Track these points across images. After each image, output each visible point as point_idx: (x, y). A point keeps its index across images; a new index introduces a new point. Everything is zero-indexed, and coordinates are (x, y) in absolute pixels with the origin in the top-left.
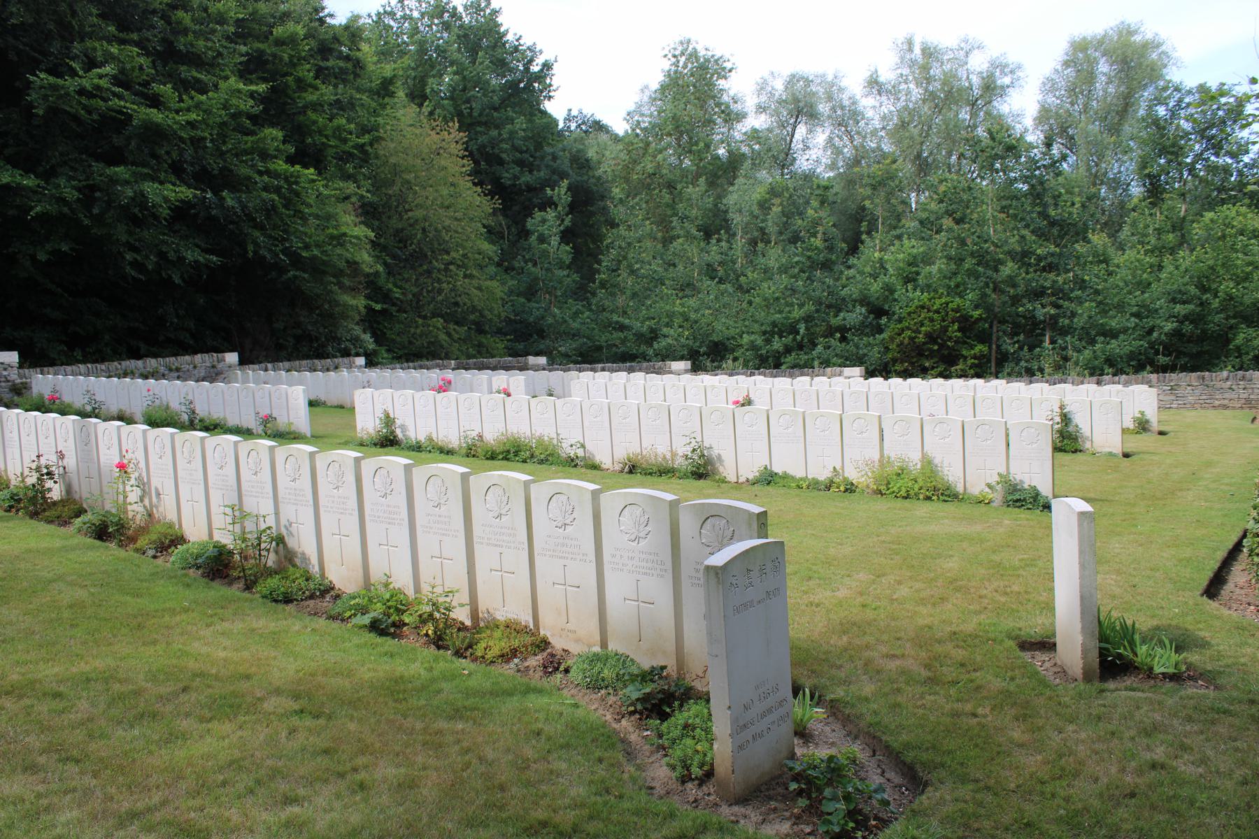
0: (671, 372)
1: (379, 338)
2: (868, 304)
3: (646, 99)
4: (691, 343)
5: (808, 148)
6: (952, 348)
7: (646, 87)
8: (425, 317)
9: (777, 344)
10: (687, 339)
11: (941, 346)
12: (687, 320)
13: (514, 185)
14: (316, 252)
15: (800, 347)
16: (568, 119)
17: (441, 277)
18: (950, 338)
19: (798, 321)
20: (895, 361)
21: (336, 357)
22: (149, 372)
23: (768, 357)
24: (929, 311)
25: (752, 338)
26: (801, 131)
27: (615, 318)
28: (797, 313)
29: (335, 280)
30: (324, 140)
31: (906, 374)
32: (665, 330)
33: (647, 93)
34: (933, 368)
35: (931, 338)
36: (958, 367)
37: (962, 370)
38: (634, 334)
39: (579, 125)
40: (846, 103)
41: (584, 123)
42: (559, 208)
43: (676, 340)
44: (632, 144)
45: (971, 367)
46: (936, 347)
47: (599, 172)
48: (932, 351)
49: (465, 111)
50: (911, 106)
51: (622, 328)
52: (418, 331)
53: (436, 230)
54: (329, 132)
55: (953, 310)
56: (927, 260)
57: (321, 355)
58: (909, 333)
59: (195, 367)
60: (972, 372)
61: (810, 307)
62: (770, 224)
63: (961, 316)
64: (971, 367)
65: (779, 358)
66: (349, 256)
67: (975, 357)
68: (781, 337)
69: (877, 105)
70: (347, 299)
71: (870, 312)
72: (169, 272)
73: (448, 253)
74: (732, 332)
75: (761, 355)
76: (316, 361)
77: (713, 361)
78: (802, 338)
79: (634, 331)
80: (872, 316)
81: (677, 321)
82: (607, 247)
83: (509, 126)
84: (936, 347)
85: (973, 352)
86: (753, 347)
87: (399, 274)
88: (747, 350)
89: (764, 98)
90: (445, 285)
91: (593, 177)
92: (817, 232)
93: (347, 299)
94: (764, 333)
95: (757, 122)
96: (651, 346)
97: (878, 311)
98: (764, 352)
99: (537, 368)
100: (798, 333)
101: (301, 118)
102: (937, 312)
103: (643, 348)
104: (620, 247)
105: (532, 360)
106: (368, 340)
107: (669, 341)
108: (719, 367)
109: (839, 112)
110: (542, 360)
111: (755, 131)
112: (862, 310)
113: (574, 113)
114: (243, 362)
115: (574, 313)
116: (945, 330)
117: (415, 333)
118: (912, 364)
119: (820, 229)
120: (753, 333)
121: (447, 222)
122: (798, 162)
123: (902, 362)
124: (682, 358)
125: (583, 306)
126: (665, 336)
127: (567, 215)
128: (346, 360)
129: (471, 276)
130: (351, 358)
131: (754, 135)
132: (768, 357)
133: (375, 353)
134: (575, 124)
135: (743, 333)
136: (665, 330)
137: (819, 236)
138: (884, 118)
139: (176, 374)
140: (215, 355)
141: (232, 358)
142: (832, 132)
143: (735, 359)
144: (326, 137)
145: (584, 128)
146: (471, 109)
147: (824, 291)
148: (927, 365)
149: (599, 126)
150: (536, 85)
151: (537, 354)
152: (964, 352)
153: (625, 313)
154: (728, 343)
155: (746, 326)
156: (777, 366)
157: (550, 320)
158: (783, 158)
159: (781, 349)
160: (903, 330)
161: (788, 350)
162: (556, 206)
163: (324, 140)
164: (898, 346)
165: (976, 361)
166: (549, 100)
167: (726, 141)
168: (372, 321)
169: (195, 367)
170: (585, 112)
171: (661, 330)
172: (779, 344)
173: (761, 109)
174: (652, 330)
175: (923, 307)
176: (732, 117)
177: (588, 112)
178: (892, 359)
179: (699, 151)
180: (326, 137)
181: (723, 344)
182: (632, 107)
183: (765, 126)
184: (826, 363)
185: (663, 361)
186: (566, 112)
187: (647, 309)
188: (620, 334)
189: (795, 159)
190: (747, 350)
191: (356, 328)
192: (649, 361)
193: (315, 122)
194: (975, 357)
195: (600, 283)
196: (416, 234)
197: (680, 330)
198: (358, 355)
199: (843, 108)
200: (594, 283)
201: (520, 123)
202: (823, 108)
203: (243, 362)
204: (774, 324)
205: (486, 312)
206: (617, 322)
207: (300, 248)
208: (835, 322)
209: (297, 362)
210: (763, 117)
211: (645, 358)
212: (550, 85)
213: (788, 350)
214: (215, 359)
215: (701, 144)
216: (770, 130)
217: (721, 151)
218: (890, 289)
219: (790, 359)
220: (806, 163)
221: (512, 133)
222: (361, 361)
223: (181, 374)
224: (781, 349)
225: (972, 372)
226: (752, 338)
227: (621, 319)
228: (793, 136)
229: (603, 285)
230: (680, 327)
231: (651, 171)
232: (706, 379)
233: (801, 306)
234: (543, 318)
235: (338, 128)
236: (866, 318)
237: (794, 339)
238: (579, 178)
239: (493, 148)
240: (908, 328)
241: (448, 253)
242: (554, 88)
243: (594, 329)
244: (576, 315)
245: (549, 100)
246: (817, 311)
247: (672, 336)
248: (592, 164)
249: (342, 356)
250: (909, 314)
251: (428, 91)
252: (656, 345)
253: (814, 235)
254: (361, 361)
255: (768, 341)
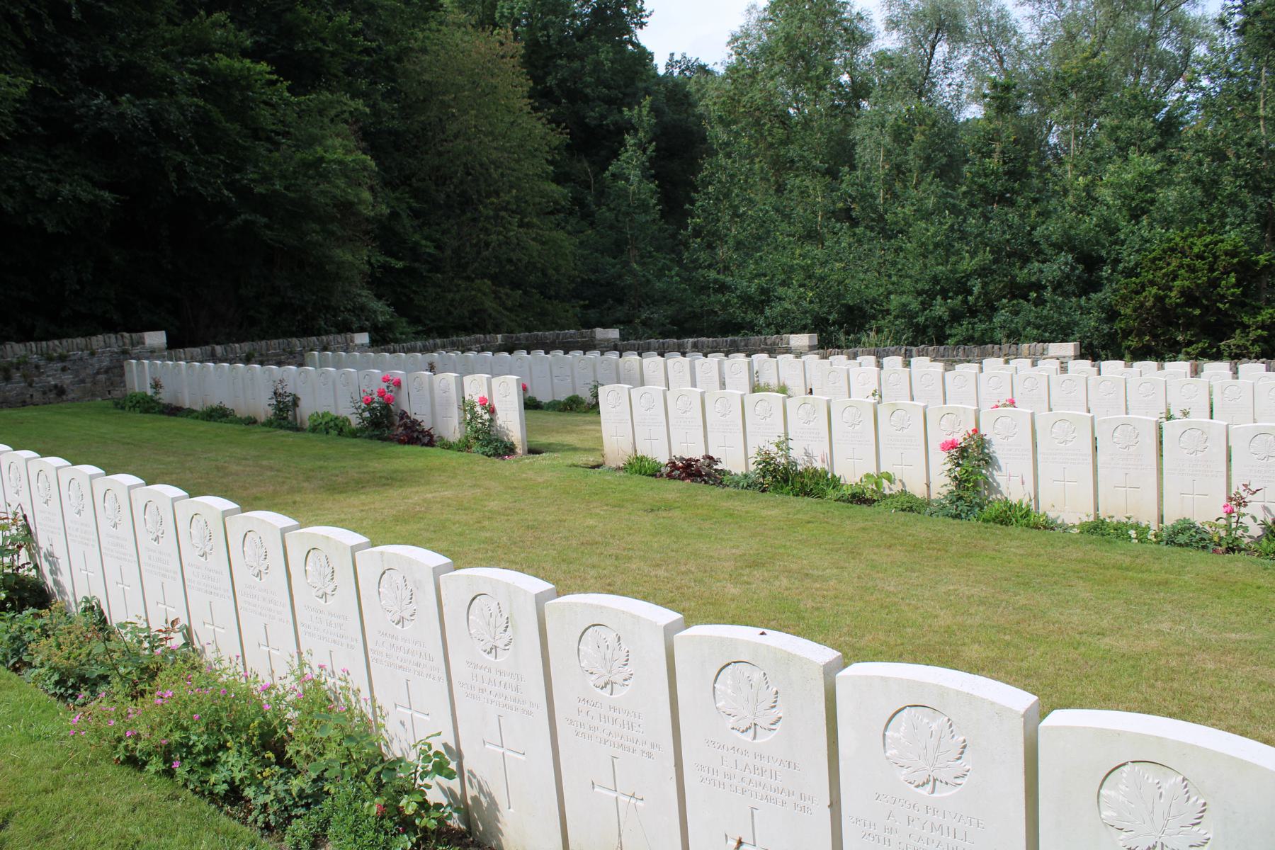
0: (788, 351)
1: (402, 307)
2: (1072, 250)
3: (753, 21)
4: (816, 307)
5: (951, 70)
6: (1225, 313)
7: (754, 7)
8: (469, 279)
9: (940, 309)
10: (811, 302)
11: (1206, 310)
12: (810, 277)
13: (601, 126)
14: (278, 186)
15: (973, 312)
16: (671, 64)
17: (489, 226)
18: (1223, 297)
19: (968, 276)
20: (1127, 333)
21: (327, 333)
22: (11, 364)
23: (928, 327)
24: (1184, 255)
25: (904, 299)
26: (942, 49)
27: (713, 274)
28: (968, 264)
29: (318, 228)
30: (320, 44)
31: (1141, 354)
32: (781, 291)
33: (755, 15)
34: (1189, 344)
35: (1190, 298)
36: (1232, 341)
37: (1238, 347)
38: (738, 297)
39: (683, 70)
40: (993, 16)
41: (687, 68)
42: (641, 134)
43: (796, 303)
44: (738, 71)
45: (1254, 342)
46: (1197, 312)
47: (700, 109)
48: (1189, 317)
49: (541, 39)
50: (1079, 13)
51: (723, 288)
52: (458, 297)
53: (481, 165)
54: (325, 35)
55: (1226, 253)
56: (1163, 178)
57: (307, 329)
58: (1154, 290)
59: (93, 354)
60: (1257, 349)
61: (985, 256)
62: (911, 156)
63: (1239, 263)
64: (1254, 342)
65: (942, 328)
66: (338, 192)
67: (1263, 327)
68: (945, 298)
69: (1035, 13)
70: (343, 255)
71: (1077, 260)
72: (40, 216)
73: (497, 194)
74: (873, 293)
75: (918, 324)
76: (295, 341)
77: (848, 333)
78: (977, 299)
79: (738, 293)
80: (1081, 267)
81: (798, 277)
82: (702, 181)
83: (594, 56)
84: (1197, 312)
85: (1260, 318)
86: (905, 312)
87: (438, 224)
88: (896, 317)
89: (897, 11)
90: (494, 237)
91: (694, 116)
92: (993, 151)
93: (343, 255)
94: (919, 293)
95: (887, 41)
96: (762, 312)
97: (1090, 261)
98: (921, 319)
99: (606, 347)
100: (970, 292)
101: (289, 16)
102: (1200, 256)
103: (750, 316)
104: (720, 182)
105: (600, 333)
106: (382, 310)
107: (787, 305)
108: (858, 342)
109: (985, 29)
110: (614, 334)
111: (882, 53)
112: (1066, 257)
113: (677, 57)
114: (174, 343)
115: (660, 270)
116: (1214, 283)
117: (453, 300)
118: (1155, 337)
119: (997, 147)
120: (903, 293)
121: (495, 155)
122: (938, 88)
123: (1140, 334)
124: (803, 329)
125: (672, 260)
126: (780, 299)
127: (650, 142)
128: (340, 338)
129: (529, 225)
130: (349, 335)
131: (884, 59)
132: (928, 327)
133: (389, 326)
134: (678, 70)
135: (890, 293)
136: (781, 291)
137: (995, 155)
138: (1044, 30)
139: (60, 365)
140: (126, 335)
141: (156, 339)
142: (974, 54)
143: (879, 331)
144: (323, 41)
145: (688, 73)
146: (549, 36)
147: (1004, 232)
148: (1180, 338)
149: (703, 69)
150: (625, 10)
151: (605, 326)
152: (1245, 319)
153: (726, 268)
154: (867, 307)
155: (893, 284)
156: (941, 340)
157: (629, 279)
158: (921, 85)
159: (946, 317)
160: (1143, 287)
161: (956, 317)
162: (636, 131)
163: (320, 44)
164: (1135, 310)
165: (1265, 333)
166: (641, 28)
167: (851, 67)
168: (380, 281)
169: (93, 354)
170: (688, 56)
171: (774, 290)
172: (943, 309)
173: (892, 24)
174: (763, 291)
175: (1173, 250)
176: (857, 37)
177: (692, 56)
178: (1123, 331)
179: (818, 77)
180: (323, 41)
181: (861, 309)
182: (737, 30)
183: (899, 45)
184: (1015, 336)
185: (778, 333)
186: (668, 57)
187: (756, 263)
188: (720, 296)
189: (934, 84)
190: (896, 317)
191: (365, 293)
192: (759, 333)
193: (306, 21)
194: (1263, 327)
195: (694, 229)
196: (456, 172)
197: (802, 290)
198: (362, 330)
199: (989, 23)
200: (686, 229)
201: (605, 54)
202: (969, 23)
203: (174, 343)
204: (935, 280)
205: (551, 272)
206: (716, 281)
207: (253, 181)
208: (1022, 275)
209: (264, 343)
210: (895, 34)
211: (752, 328)
212: (641, 10)
213: (956, 317)
214: (127, 341)
215: (821, 69)
216: (904, 50)
217: (845, 78)
218: (1109, 228)
219: (960, 330)
220: (947, 89)
221: (598, 65)
222: (363, 338)
223: (67, 364)
224: (946, 317)
225: (1257, 349)
226: (904, 299)
227: (721, 277)
228: (932, 54)
229: (697, 233)
230: (800, 286)
231: (760, 102)
232: (839, 361)
233: (973, 254)
234: (620, 277)
235: (341, 28)
236: (1073, 269)
237: (965, 301)
238: (676, 117)
239: (575, 83)
240: (1152, 283)
241: (497, 194)
242: (647, 13)
243: (685, 290)
244: (660, 274)
245: (641, 28)
246: (996, 261)
247: (789, 298)
248: (692, 100)
249: (339, 332)
250: (1154, 260)
251: (497, 15)
252: (768, 312)
253: (989, 155)
254: (363, 338)
255: (925, 306)
